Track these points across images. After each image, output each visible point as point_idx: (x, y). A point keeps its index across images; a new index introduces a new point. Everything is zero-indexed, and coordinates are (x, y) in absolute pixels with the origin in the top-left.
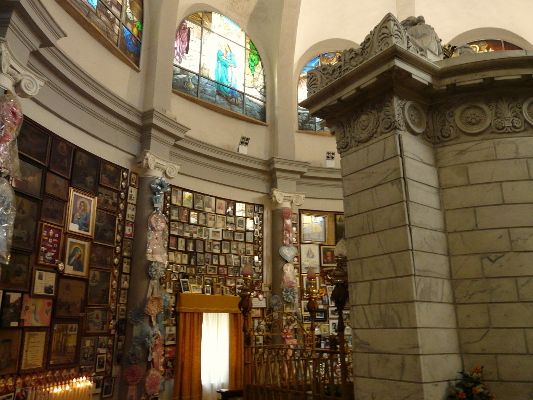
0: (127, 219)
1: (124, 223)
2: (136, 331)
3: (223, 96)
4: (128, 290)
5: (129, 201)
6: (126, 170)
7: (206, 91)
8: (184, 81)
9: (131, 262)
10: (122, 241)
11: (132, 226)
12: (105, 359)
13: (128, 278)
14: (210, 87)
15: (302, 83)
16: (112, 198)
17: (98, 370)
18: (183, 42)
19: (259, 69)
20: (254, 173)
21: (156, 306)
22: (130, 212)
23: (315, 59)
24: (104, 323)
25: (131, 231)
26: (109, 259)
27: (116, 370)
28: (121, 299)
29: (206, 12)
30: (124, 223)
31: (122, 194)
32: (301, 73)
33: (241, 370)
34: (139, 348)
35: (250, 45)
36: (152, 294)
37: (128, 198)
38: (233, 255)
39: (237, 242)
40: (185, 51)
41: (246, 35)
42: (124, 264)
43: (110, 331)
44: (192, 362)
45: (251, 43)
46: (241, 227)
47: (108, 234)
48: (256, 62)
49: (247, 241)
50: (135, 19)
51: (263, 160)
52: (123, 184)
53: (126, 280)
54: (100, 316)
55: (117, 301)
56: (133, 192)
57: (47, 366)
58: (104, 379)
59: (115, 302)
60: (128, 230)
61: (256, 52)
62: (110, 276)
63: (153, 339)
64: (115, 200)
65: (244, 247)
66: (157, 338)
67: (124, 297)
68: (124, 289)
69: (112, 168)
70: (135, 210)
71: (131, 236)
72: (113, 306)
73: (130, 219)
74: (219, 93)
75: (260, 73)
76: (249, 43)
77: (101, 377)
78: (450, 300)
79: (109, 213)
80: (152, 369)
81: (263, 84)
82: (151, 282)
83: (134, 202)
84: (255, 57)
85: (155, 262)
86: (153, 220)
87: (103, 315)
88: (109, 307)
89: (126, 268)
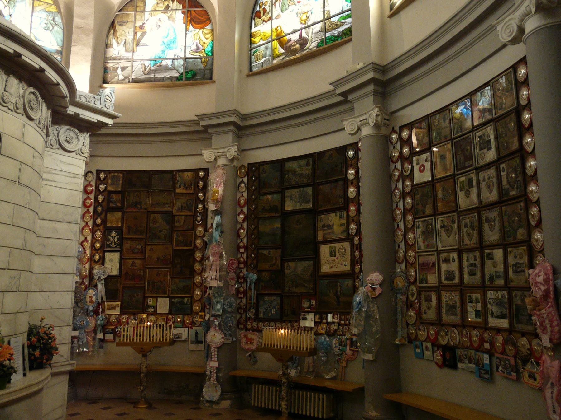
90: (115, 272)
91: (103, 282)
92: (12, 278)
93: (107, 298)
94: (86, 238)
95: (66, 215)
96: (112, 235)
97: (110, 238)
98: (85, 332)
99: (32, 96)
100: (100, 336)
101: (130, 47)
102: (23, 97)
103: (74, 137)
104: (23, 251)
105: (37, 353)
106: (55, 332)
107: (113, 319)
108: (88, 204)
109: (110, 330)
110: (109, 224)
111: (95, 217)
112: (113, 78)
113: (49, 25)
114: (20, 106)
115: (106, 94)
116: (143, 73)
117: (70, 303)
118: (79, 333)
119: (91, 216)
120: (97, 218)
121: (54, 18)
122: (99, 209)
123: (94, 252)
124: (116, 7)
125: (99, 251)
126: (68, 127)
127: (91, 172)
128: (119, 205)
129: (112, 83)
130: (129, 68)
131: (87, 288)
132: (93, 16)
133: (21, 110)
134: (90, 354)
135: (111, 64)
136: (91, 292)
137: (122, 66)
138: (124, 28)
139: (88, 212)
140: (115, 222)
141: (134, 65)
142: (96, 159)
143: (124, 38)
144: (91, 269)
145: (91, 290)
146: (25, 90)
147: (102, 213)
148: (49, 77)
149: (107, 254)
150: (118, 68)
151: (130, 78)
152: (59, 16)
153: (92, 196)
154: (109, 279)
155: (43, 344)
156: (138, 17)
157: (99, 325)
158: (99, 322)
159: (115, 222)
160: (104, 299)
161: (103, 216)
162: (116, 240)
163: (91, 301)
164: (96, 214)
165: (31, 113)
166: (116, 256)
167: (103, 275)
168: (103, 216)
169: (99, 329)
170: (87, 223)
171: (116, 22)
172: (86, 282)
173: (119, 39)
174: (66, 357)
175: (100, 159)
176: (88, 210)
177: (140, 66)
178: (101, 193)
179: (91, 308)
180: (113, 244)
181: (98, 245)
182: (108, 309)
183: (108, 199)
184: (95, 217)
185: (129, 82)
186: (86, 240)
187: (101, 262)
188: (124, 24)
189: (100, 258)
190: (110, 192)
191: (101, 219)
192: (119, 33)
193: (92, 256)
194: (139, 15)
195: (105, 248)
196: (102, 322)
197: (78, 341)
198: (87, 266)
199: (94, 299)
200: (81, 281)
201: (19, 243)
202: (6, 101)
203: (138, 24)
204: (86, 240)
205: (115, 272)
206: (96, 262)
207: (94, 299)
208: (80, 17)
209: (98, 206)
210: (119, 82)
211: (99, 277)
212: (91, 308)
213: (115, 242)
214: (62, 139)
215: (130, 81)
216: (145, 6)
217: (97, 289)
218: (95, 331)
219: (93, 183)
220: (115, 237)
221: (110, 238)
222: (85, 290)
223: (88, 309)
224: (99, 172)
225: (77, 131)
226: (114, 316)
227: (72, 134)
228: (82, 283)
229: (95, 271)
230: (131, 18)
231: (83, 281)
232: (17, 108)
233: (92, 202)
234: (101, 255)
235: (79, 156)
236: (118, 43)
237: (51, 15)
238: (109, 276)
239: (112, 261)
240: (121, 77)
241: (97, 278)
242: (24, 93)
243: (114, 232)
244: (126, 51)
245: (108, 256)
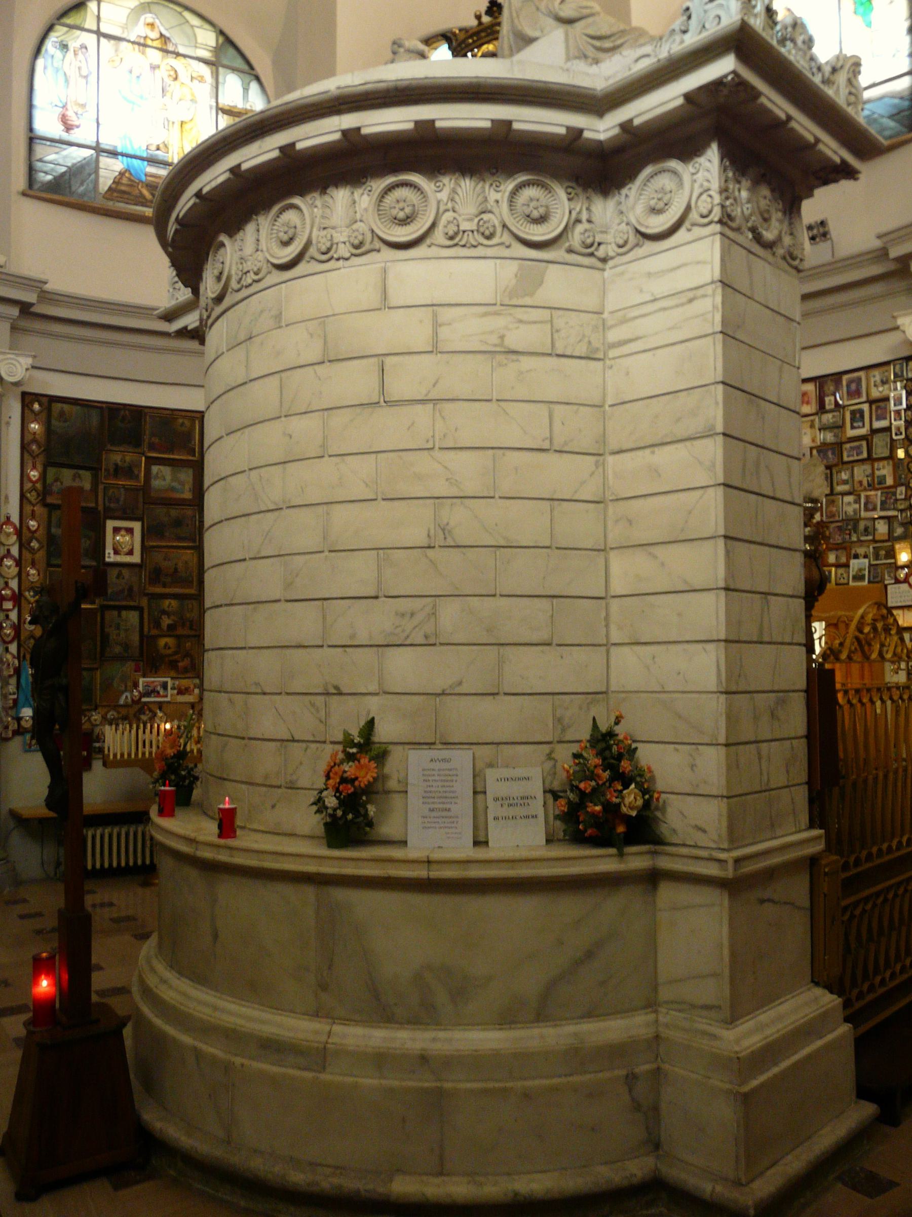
20: (877, 289)
33: (886, 725)
38: (833, 569)
39: (850, 466)
44: (636, 1010)
46: (859, 427)
49: (874, 456)
51: (877, 250)
57: (198, 677)
65: (869, 471)
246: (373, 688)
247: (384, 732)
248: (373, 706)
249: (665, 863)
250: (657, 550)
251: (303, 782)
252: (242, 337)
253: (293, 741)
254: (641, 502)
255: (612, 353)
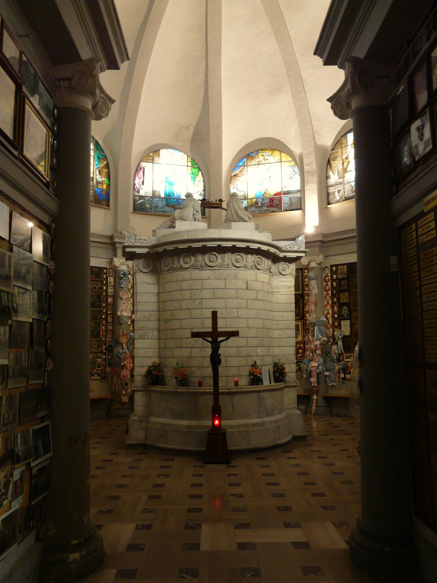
0: (108, 294)
1: (107, 297)
2: (116, 351)
3: (170, 206)
4: (112, 330)
5: (109, 284)
6: (106, 268)
7: (157, 206)
8: (142, 204)
9: (113, 316)
10: (106, 306)
11: (112, 298)
12: (101, 364)
13: (112, 325)
14: (160, 203)
15: (233, 180)
16: (98, 285)
17: (97, 369)
18: (140, 178)
19: (200, 178)
21: (126, 338)
22: (110, 290)
23: (243, 159)
24: (98, 347)
25: (112, 300)
26: (99, 316)
27: (108, 369)
28: (108, 336)
29: (155, 151)
30: (107, 296)
31: (105, 282)
32: (232, 172)
34: (117, 359)
35: (191, 162)
36: (123, 332)
37: (108, 283)
40: (142, 184)
41: (188, 156)
42: (109, 318)
43: (103, 351)
45: (192, 161)
47: (97, 304)
48: (196, 174)
50: (104, 179)
52: (104, 276)
53: (111, 326)
54: (96, 344)
55: (106, 336)
56: (111, 280)
58: (101, 373)
59: (105, 337)
60: (110, 300)
61: (197, 166)
62: (100, 324)
63: (123, 355)
64: (100, 286)
66: (126, 354)
67: (110, 334)
68: (110, 330)
69: (97, 270)
70: (113, 289)
71: (112, 303)
72: (104, 339)
73: (110, 294)
74: (168, 205)
75: (200, 181)
76: (190, 161)
77: (100, 372)
78: (157, 338)
79: (97, 293)
80: (124, 369)
81: (203, 188)
82: (122, 326)
83: (113, 284)
84: (196, 170)
85: (123, 316)
86: (121, 294)
87: (98, 344)
88: (102, 340)
89: (110, 319)
90: (348, 333)
91: (341, 340)
92: (259, 341)
93: (344, 351)
94: (328, 312)
95: (287, 308)
96: (344, 308)
97: (343, 310)
98: (333, 373)
99: (259, 259)
100: (342, 375)
101: (341, 175)
102: (254, 261)
103: (287, 267)
104: (263, 329)
105: (277, 375)
106: (285, 366)
107: (349, 364)
108: (327, 289)
109: (348, 372)
110: (341, 301)
111: (333, 297)
112: (333, 200)
113: (292, 175)
114: (253, 266)
115: (300, 240)
116: (351, 192)
117: (294, 352)
118: (329, 373)
119: (330, 297)
120: (334, 298)
121: (294, 169)
122: (335, 292)
123: (334, 320)
124: (330, 148)
125: (337, 320)
126: (283, 263)
127: (327, 267)
128: (346, 287)
129: (333, 204)
130: (342, 191)
131: (332, 344)
132: (315, 161)
133: (254, 268)
134: (337, 387)
135: (331, 190)
136: (334, 347)
137: (338, 190)
138: (336, 162)
139: (328, 294)
140: (345, 300)
141: (345, 187)
142: (329, 258)
143: (336, 169)
144: (333, 331)
145: (334, 346)
146: (255, 258)
147: (336, 294)
148: (3, 554)
149: (342, 322)
150: (335, 192)
151: (344, 197)
152: (296, 166)
153: (329, 283)
154: (344, 338)
155: (280, 371)
156: (344, 151)
157: (341, 368)
158: (340, 367)
159: (345, 300)
160: (343, 352)
161: (337, 296)
162: (347, 312)
163: (335, 353)
164: (333, 295)
165: (259, 267)
166: (348, 322)
167: (341, 336)
168: (337, 296)
169: (341, 371)
170: (328, 302)
171: (331, 159)
172: (331, 340)
173: (334, 171)
174: (294, 379)
175: (331, 257)
176: (328, 293)
177: (349, 187)
178: (334, 280)
179: (335, 358)
180: (345, 314)
181: (336, 316)
182: (346, 358)
183: (339, 284)
184: (333, 297)
185: (343, 201)
186: (328, 313)
187: (339, 327)
188: (336, 159)
189: (338, 324)
190: (340, 279)
191: (336, 298)
192: (333, 167)
193: (333, 323)
194: (344, 150)
195: (341, 318)
196: (342, 366)
197: (329, 378)
198: (331, 330)
199: (336, 351)
200: (328, 340)
201: (261, 326)
202: (247, 266)
203: (344, 157)
204: (328, 313)
205: (348, 333)
206: (336, 327)
207: (336, 351)
208: (308, 165)
209: (333, 289)
210: (337, 202)
211: (338, 337)
212: (335, 358)
213: (346, 313)
214: (280, 270)
215: (344, 199)
216: (347, 142)
217: (338, 345)
218: (339, 372)
219: (329, 275)
220: (346, 310)
221: (343, 310)
222: (331, 346)
223: (333, 358)
224: (332, 266)
225: (287, 263)
226: (350, 362)
227: (285, 266)
228: (329, 341)
229: (335, 333)
230: (340, 154)
231: (329, 340)
232: (252, 268)
233: (329, 288)
234: (339, 322)
235: (290, 276)
236: (334, 174)
237: (292, 168)
238: (345, 336)
239: (346, 326)
240: (338, 198)
241: (337, 337)
242: (254, 259)
243: (345, 307)
244: (339, 178)
245: (343, 322)
246: (255, 355)
247: (258, 363)
248: (255, 358)
249: (287, 384)
250: (283, 330)
251: (243, 374)
252: (222, 277)
253: (241, 366)
254: (280, 321)
255: (274, 293)
